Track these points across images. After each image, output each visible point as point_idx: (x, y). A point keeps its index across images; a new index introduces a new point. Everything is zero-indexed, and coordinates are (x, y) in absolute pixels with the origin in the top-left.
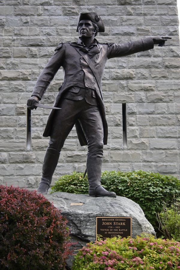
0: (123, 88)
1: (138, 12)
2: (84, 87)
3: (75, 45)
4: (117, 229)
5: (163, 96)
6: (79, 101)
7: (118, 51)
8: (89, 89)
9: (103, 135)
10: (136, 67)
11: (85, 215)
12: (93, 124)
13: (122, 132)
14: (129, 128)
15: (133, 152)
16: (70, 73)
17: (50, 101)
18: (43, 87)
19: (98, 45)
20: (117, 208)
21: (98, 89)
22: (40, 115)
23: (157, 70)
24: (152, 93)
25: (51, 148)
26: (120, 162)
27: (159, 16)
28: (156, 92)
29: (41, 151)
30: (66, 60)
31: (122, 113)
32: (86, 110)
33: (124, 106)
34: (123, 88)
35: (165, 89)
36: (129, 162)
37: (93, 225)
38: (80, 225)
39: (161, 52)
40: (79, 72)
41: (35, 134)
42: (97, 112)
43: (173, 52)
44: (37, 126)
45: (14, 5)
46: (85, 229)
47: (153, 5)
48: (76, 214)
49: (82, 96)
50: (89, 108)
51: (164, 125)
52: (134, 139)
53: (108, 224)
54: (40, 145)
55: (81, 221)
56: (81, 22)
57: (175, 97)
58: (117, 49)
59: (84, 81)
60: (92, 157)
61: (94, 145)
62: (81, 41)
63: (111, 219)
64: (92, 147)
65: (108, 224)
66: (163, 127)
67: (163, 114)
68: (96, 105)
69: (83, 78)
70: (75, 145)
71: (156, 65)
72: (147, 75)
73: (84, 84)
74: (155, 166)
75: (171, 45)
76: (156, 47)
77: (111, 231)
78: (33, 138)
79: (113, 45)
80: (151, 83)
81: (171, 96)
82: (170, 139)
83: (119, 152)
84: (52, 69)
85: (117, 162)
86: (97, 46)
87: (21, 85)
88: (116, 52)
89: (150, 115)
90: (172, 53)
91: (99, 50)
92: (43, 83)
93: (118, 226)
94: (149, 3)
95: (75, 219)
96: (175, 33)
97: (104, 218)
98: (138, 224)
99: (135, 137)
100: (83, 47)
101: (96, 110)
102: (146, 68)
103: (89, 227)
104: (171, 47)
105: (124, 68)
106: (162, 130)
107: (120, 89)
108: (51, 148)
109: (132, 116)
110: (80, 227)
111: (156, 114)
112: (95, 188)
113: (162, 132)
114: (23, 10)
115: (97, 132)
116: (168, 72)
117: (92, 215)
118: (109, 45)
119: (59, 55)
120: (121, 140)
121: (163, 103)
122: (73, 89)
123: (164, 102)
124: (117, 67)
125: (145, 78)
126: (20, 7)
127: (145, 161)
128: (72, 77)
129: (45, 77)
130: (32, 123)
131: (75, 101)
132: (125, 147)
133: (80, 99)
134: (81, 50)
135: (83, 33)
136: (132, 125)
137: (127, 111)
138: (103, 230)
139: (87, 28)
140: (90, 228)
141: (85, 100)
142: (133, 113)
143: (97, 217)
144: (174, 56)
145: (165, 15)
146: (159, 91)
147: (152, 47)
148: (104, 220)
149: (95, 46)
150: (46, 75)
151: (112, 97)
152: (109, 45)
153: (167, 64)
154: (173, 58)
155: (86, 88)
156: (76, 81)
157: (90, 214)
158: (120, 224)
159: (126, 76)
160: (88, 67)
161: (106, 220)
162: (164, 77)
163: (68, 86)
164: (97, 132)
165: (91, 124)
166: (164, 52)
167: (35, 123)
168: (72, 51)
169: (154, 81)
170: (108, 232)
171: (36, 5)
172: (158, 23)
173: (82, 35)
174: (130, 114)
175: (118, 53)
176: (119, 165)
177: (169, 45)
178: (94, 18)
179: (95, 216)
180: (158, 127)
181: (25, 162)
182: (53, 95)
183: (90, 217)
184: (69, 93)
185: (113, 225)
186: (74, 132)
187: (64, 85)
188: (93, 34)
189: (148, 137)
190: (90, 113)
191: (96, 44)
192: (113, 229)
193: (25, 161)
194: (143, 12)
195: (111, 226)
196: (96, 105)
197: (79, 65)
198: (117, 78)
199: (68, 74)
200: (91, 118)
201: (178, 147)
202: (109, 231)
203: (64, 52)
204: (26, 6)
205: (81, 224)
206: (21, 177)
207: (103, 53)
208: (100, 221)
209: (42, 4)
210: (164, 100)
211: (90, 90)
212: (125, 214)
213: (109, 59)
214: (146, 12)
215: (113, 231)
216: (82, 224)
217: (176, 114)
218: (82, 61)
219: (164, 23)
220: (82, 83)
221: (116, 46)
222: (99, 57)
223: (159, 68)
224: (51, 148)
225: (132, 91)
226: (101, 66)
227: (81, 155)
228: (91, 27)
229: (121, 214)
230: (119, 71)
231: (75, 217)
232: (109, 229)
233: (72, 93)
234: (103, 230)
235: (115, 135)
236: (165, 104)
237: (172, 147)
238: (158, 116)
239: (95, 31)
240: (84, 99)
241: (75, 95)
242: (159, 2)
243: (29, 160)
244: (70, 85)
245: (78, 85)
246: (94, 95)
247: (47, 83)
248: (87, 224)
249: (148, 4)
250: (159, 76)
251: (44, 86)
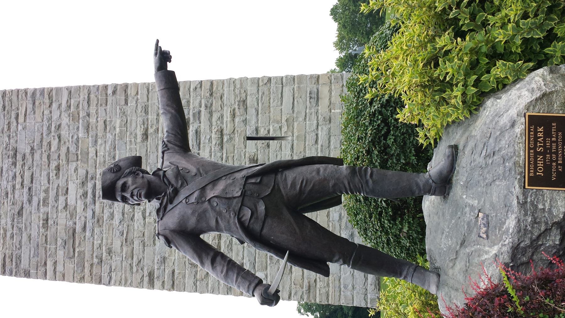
0: (231, 139)
1: (155, 122)
2: (241, 199)
3: (162, 211)
4: (551, 145)
6: (266, 208)
7: (178, 133)
8: (244, 188)
9: (330, 166)
10: (211, 126)
11: (520, 212)
12: (309, 183)
13: (276, 141)
14: (271, 135)
15: (295, 130)
16: (213, 223)
18: (238, 274)
19: (165, 170)
20: (503, 142)
21: (244, 173)
25: (350, 262)
26: (305, 144)
30: (189, 229)
31: (256, 141)
32: (282, 195)
33: (249, 138)
34: (231, 139)
35: (233, 97)
36: (305, 135)
37: (543, 196)
38: (543, 225)
39: (196, 100)
40: (213, 208)
42: (287, 176)
43: (196, 88)
45: (144, 246)
46: (553, 214)
48: (519, 231)
49: (258, 202)
51: (270, 98)
52: (283, 129)
53: (540, 164)
55: (535, 222)
56: (119, 199)
57: (241, 87)
58: (173, 136)
59: (229, 199)
60: (371, 187)
61: (349, 183)
62: (155, 200)
63: (529, 158)
64: (351, 185)
65: (540, 164)
66: (272, 100)
67: (258, 100)
69: (223, 200)
71: (209, 105)
72: (219, 115)
73: (235, 198)
74: (310, 109)
76: (170, 67)
77: (557, 157)
79: (166, 143)
80: (227, 111)
82: (284, 93)
83: (295, 144)
85: (305, 147)
86: (165, 172)
87: (225, 241)
88: (179, 136)
90: (198, 89)
91: (173, 167)
92: (230, 273)
93: (544, 140)
95: (530, 235)
97: (529, 173)
98: (541, 99)
99: (280, 128)
100: (166, 197)
101: (284, 176)
102: (212, 116)
103: (547, 205)
104: (191, 90)
105: (211, 137)
107: (232, 142)
108: (351, 262)
109: (260, 131)
110: (546, 223)
112: (433, 185)
114: (149, 237)
115: (324, 176)
116: (216, 94)
117: (521, 197)
118: (166, 149)
120: (283, 142)
122: (243, 219)
123: (246, 98)
124: (210, 144)
125: (222, 116)
126: (146, 240)
127: (305, 119)
128: (222, 220)
129: (219, 268)
131: (266, 215)
132: (290, 138)
133: (264, 208)
134: (171, 201)
135: (140, 196)
136: (269, 131)
137: (254, 135)
138: (554, 175)
139: (131, 188)
140: (550, 202)
142: (257, 130)
143: (527, 187)
144: (201, 87)
147: (172, 75)
148: (532, 171)
149: (164, 175)
150: (215, 267)
151: (240, 150)
152: (166, 149)
155: (243, 194)
156: (230, 213)
157: (518, 203)
158: (541, 137)
159: (220, 136)
160: (203, 189)
161: (532, 167)
162: (221, 98)
163: (237, 228)
164: (324, 176)
168: (171, 220)
169: (225, 108)
170: (558, 165)
171: (145, 224)
173: (143, 199)
174: (257, 133)
176: (308, 145)
178: (113, 175)
179: (524, 191)
180: (271, 105)
183: (526, 202)
184: (251, 226)
185: (544, 154)
186: (319, 217)
187: (235, 235)
188: (143, 177)
191: (161, 173)
192: (551, 153)
194: (155, 117)
195: (544, 158)
196: (273, 176)
197: (199, 206)
198: (221, 145)
199: (214, 227)
200: (298, 187)
202: (556, 161)
203: (173, 231)
204: (146, 234)
205: (539, 223)
207: (178, 161)
208: (535, 181)
209: (144, 218)
211: (246, 188)
212: (520, 128)
213: (190, 150)
214: (155, 114)
215: (556, 153)
216: (541, 219)
217: (259, 86)
218: (193, 199)
220: (233, 202)
221: (168, 136)
222: (185, 168)
224: (351, 262)
225: (234, 130)
226: (203, 165)
228: (130, 180)
229: (519, 135)
230: (214, 143)
231: (525, 234)
232: (552, 161)
233: (252, 221)
234: (554, 175)
235: (278, 148)
237: (292, 91)
238: (260, 104)
239: (138, 174)
240: (262, 199)
241: (255, 216)
244: (236, 224)
245: (237, 208)
246: (257, 180)
247: (230, 265)
248: (541, 209)
250: (220, 102)
251: (236, 272)
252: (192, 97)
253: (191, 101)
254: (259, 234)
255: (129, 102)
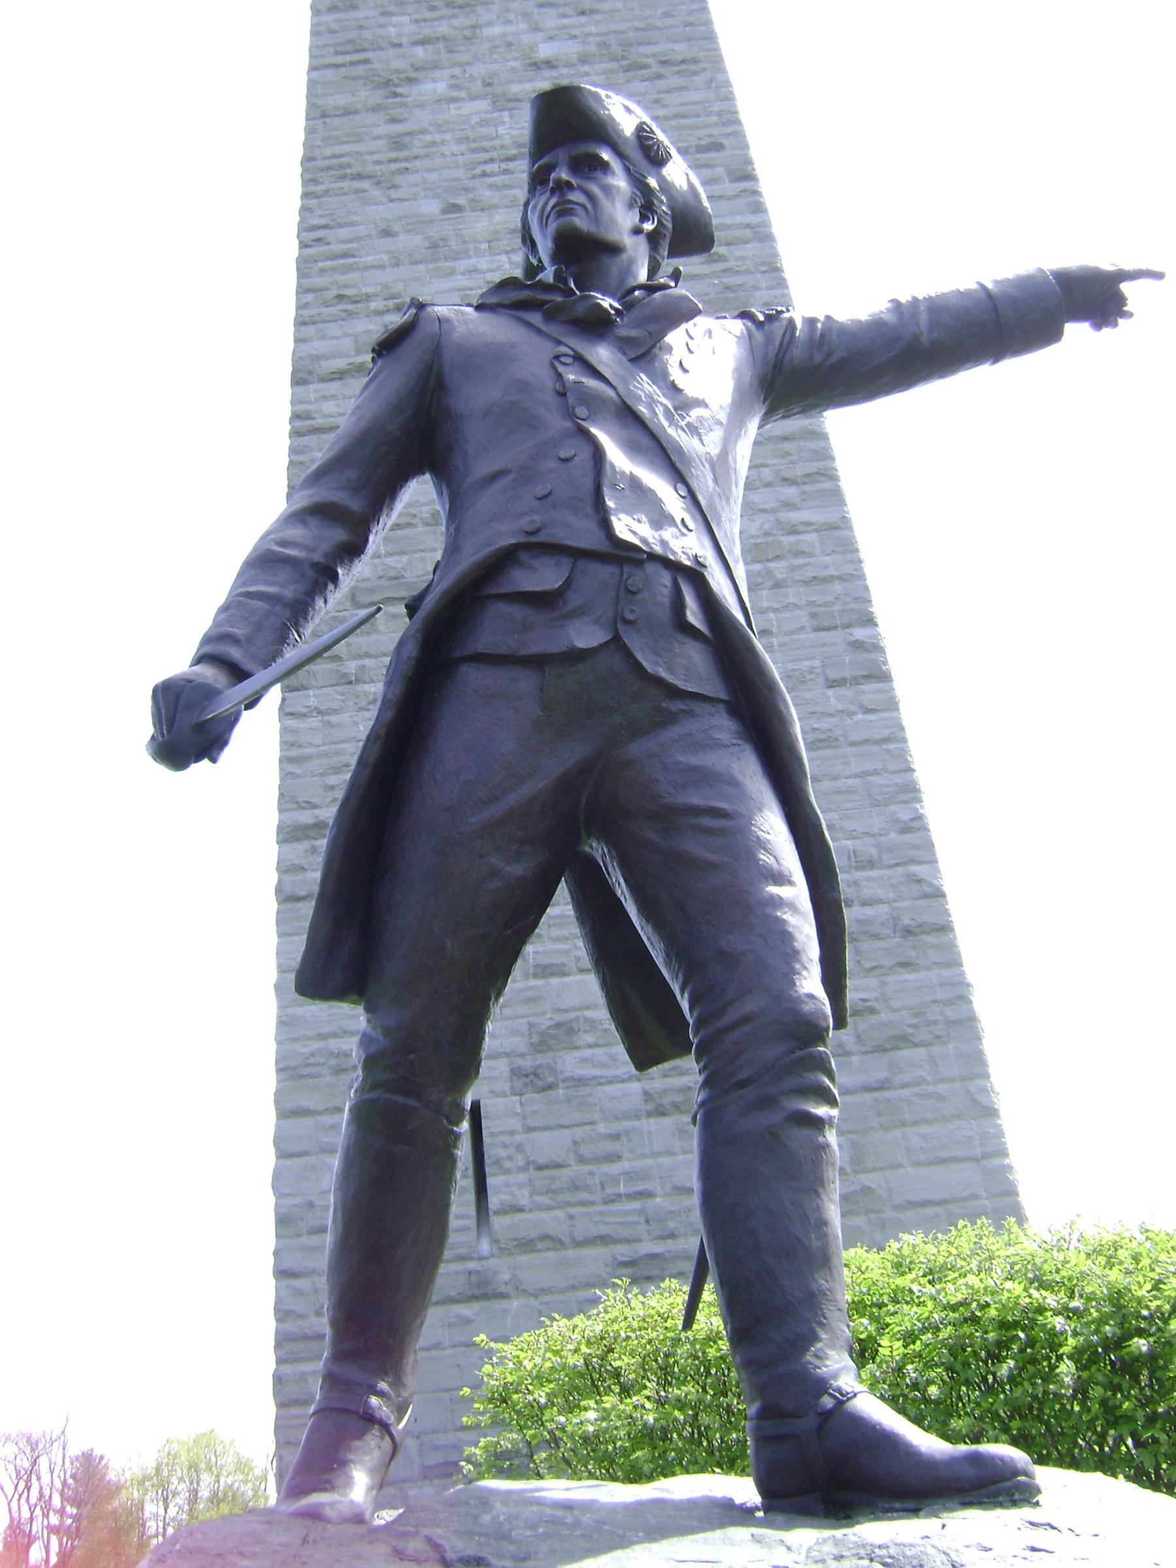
2: (604, 546)
5: (910, 1026)
17: (540, 1083)
22: (512, 1133)
23: (878, 944)
24: (873, 1019)
27: (858, 780)
28: (884, 1016)
29: (525, 1252)
41: (503, 1197)
44: (508, 1171)
47: (834, 747)
50: (671, 719)
51: (927, 1122)
54: (522, 1235)
66: (926, 1129)
68: (723, 695)
70: (638, 1223)
75: (913, 861)
78: (496, 1213)
81: (936, 1022)
84: (352, 474)
89: (876, 1094)
94: (822, 745)
96: (916, 824)
104: (913, 868)
106: (924, 1137)
111: (895, 1089)
113: (923, 1145)
116: (914, 947)
119: (402, 371)
121: (913, 1050)
123: (916, 1045)
130: (488, 1160)
133: (581, 643)
141: (629, 655)
145: (875, 773)
146: (896, 1010)
153: (906, 921)
154: (923, 903)
162: (904, 965)
165: (693, 846)
166: (891, 885)
167: (498, 1162)
169: (872, 981)
172: (857, 801)
175: (833, 360)
177: (905, 863)
180: (907, 1130)
181: (475, 1298)
182: (551, 1062)
189: (881, 1169)
190: (681, 759)
193: (477, 1292)
196: (723, 695)
200: (696, 800)
201: (986, 1190)
206: (466, 1349)
210: (915, 1040)
219: (879, 798)
223: (882, 939)
227: (663, 1254)
236: (921, 1050)
237: (966, 1193)
242: (851, 739)
243: (489, 1290)
249: (819, 748)
250: (887, 962)
252: (888, 872)
253: (875, 873)
254: (457, 654)
255: (839, 691)
